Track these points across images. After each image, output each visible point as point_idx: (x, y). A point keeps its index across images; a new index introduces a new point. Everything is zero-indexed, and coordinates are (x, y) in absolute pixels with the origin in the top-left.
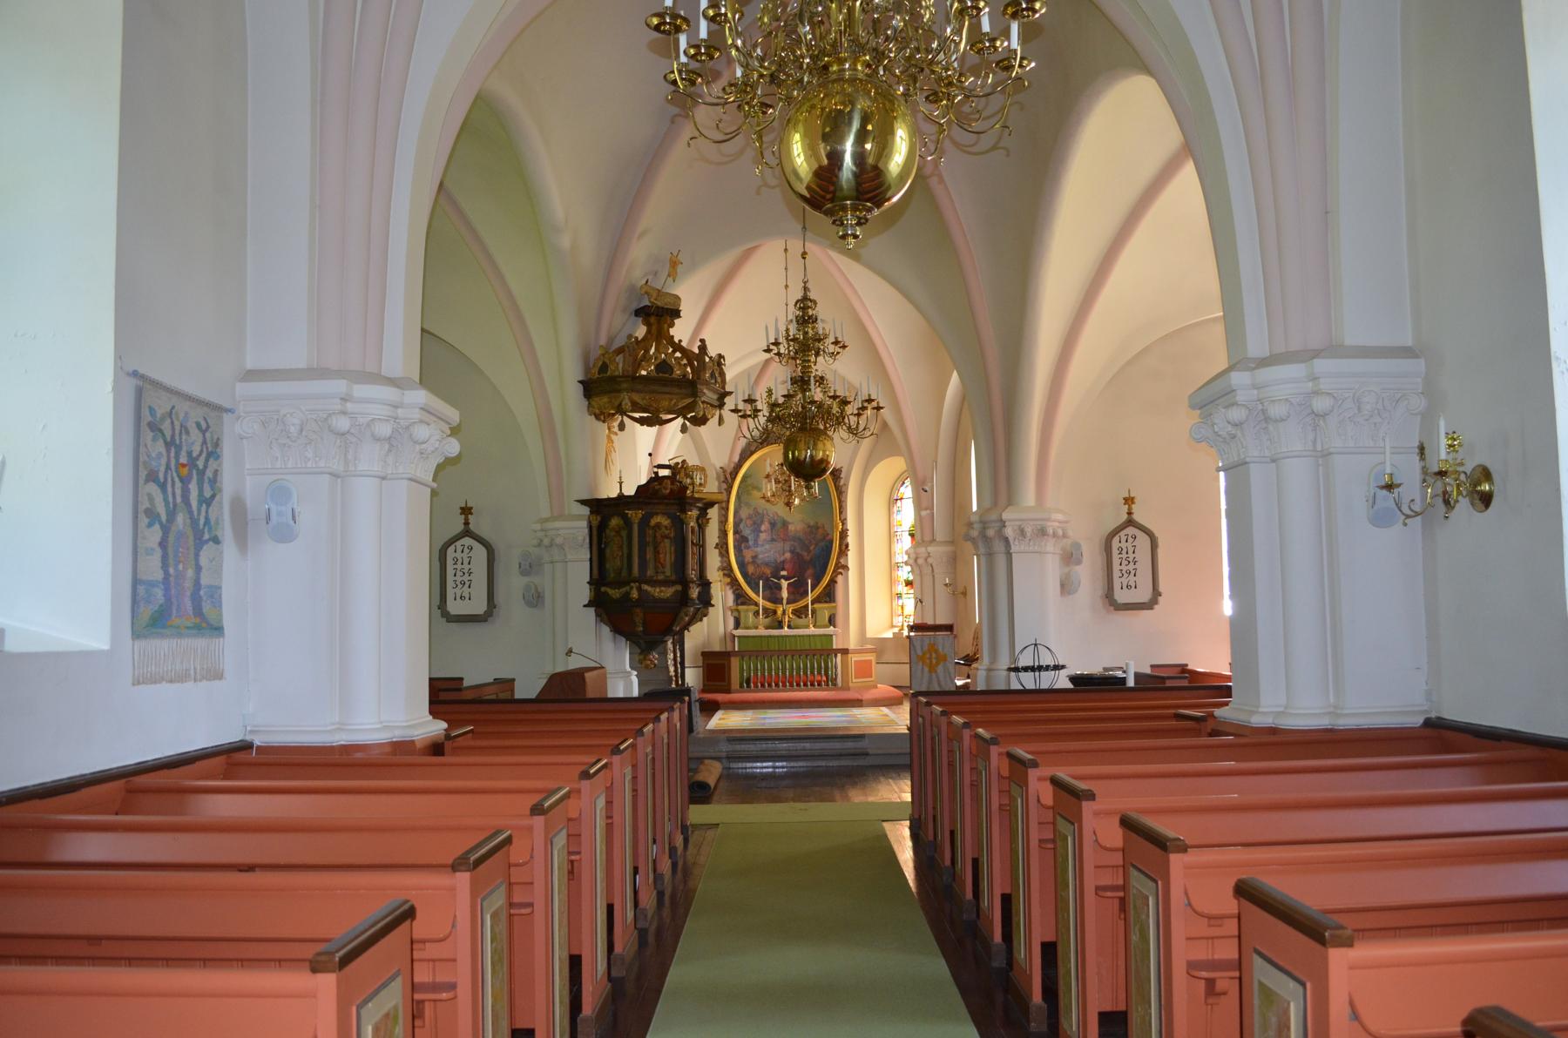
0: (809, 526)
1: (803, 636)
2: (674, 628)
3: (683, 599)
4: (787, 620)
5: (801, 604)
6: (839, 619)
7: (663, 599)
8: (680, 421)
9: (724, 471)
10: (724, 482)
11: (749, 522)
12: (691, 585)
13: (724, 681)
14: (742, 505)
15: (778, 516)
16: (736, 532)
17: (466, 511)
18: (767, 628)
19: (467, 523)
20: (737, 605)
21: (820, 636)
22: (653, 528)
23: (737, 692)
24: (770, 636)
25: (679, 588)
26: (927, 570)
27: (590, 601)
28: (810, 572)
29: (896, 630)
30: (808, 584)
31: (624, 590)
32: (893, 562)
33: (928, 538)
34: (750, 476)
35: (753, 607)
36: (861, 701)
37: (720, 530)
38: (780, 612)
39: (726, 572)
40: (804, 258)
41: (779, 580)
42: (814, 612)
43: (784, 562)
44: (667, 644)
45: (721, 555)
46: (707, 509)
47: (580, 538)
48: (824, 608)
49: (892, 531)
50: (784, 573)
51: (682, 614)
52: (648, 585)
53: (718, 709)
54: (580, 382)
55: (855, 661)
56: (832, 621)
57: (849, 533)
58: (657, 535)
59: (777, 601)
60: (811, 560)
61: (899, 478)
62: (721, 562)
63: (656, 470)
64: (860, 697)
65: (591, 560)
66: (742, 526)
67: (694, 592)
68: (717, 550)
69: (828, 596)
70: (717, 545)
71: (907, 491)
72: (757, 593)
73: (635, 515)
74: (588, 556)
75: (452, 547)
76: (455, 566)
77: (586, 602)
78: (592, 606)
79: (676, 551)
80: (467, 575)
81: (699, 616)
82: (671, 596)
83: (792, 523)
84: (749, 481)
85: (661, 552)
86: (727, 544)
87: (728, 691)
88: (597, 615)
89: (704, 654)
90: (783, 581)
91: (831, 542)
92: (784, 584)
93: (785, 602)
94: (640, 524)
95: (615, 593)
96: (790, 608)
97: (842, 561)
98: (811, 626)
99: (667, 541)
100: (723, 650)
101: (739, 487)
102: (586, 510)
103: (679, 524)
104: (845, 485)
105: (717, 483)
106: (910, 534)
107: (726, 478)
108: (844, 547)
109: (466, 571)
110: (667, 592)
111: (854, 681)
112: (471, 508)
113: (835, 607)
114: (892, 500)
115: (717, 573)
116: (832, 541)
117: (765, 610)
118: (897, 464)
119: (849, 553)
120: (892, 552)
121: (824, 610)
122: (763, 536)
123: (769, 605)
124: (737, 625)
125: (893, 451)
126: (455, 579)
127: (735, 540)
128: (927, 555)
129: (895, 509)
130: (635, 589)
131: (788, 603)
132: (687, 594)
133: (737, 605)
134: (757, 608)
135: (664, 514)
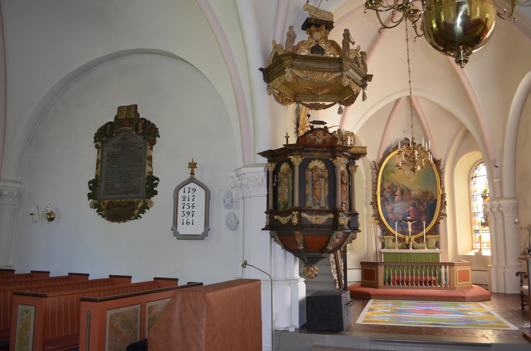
0: (423, 192)
1: (421, 253)
2: (328, 248)
3: (335, 225)
4: (411, 244)
5: (420, 235)
6: (442, 244)
7: (318, 225)
8: (337, 106)
9: (375, 163)
10: (374, 169)
11: (389, 190)
12: (341, 214)
13: (374, 280)
14: (385, 181)
15: (405, 187)
16: (381, 196)
17: (193, 165)
18: (400, 248)
19: (192, 173)
20: (383, 235)
21: (431, 253)
22: (312, 170)
23: (382, 288)
24: (402, 253)
25: (331, 216)
26: (499, 215)
27: (266, 226)
28: (424, 217)
29: (477, 251)
30: (423, 224)
31: (289, 217)
32: (472, 212)
33: (498, 195)
34: (389, 165)
35: (392, 237)
36: (465, 297)
37: (373, 194)
38: (407, 239)
39: (377, 217)
40: (410, 83)
41: (407, 222)
42: (426, 240)
43: (409, 212)
44: (329, 259)
45: (374, 208)
46: (354, 159)
47: (260, 180)
48: (433, 238)
49: (471, 195)
50: (409, 218)
51: (334, 237)
52: (307, 213)
53: (371, 298)
54: (261, 69)
55: (458, 271)
56: (437, 245)
57: (446, 196)
58: (314, 175)
59: (405, 233)
60: (425, 210)
61: (474, 164)
62: (374, 212)
63: (311, 124)
64: (463, 295)
65: (268, 195)
66: (385, 193)
67: (343, 220)
68: (371, 206)
69: (435, 231)
70: (371, 202)
71: (482, 170)
72: (394, 229)
73: (296, 160)
74: (266, 193)
75: (182, 189)
76: (184, 202)
77: (264, 227)
78: (267, 230)
79: (329, 187)
80: (191, 207)
81: (349, 238)
82: (325, 222)
83: (413, 191)
84: (389, 168)
85: (317, 188)
86: (377, 202)
87: (377, 287)
88: (272, 237)
89: (363, 264)
90: (409, 222)
91: (436, 201)
92: (410, 224)
93: (410, 234)
94: (300, 166)
95: (284, 220)
96: (413, 238)
97: (443, 211)
98: (426, 248)
99: (322, 180)
100: (376, 261)
101: (383, 172)
102: (265, 160)
103: (331, 168)
104: (443, 169)
105: (371, 170)
106: (482, 197)
107: (376, 167)
108: (443, 203)
109: (191, 205)
110: (322, 219)
111: (458, 284)
112: (196, 164)
113: (439, 237)
114: (470, 178)
115: (372, 218)
116: (437, 200)
117: (399, 238)
118: (476, 155)
119: (447, 207)
120: (471, 207)
121: (433, 239)
122: (397, 198)
123: (401, 236)
124: (383, 246)
125: (473, 147)
126: (183, 210)
127: (381, 200)
128: (498, 205)
129: (472, 183)
130: (295, 216)
131: (412, 235)
132: (338, 221)
133: (383, 235)
134: (394, 237)
135: (319, 160)
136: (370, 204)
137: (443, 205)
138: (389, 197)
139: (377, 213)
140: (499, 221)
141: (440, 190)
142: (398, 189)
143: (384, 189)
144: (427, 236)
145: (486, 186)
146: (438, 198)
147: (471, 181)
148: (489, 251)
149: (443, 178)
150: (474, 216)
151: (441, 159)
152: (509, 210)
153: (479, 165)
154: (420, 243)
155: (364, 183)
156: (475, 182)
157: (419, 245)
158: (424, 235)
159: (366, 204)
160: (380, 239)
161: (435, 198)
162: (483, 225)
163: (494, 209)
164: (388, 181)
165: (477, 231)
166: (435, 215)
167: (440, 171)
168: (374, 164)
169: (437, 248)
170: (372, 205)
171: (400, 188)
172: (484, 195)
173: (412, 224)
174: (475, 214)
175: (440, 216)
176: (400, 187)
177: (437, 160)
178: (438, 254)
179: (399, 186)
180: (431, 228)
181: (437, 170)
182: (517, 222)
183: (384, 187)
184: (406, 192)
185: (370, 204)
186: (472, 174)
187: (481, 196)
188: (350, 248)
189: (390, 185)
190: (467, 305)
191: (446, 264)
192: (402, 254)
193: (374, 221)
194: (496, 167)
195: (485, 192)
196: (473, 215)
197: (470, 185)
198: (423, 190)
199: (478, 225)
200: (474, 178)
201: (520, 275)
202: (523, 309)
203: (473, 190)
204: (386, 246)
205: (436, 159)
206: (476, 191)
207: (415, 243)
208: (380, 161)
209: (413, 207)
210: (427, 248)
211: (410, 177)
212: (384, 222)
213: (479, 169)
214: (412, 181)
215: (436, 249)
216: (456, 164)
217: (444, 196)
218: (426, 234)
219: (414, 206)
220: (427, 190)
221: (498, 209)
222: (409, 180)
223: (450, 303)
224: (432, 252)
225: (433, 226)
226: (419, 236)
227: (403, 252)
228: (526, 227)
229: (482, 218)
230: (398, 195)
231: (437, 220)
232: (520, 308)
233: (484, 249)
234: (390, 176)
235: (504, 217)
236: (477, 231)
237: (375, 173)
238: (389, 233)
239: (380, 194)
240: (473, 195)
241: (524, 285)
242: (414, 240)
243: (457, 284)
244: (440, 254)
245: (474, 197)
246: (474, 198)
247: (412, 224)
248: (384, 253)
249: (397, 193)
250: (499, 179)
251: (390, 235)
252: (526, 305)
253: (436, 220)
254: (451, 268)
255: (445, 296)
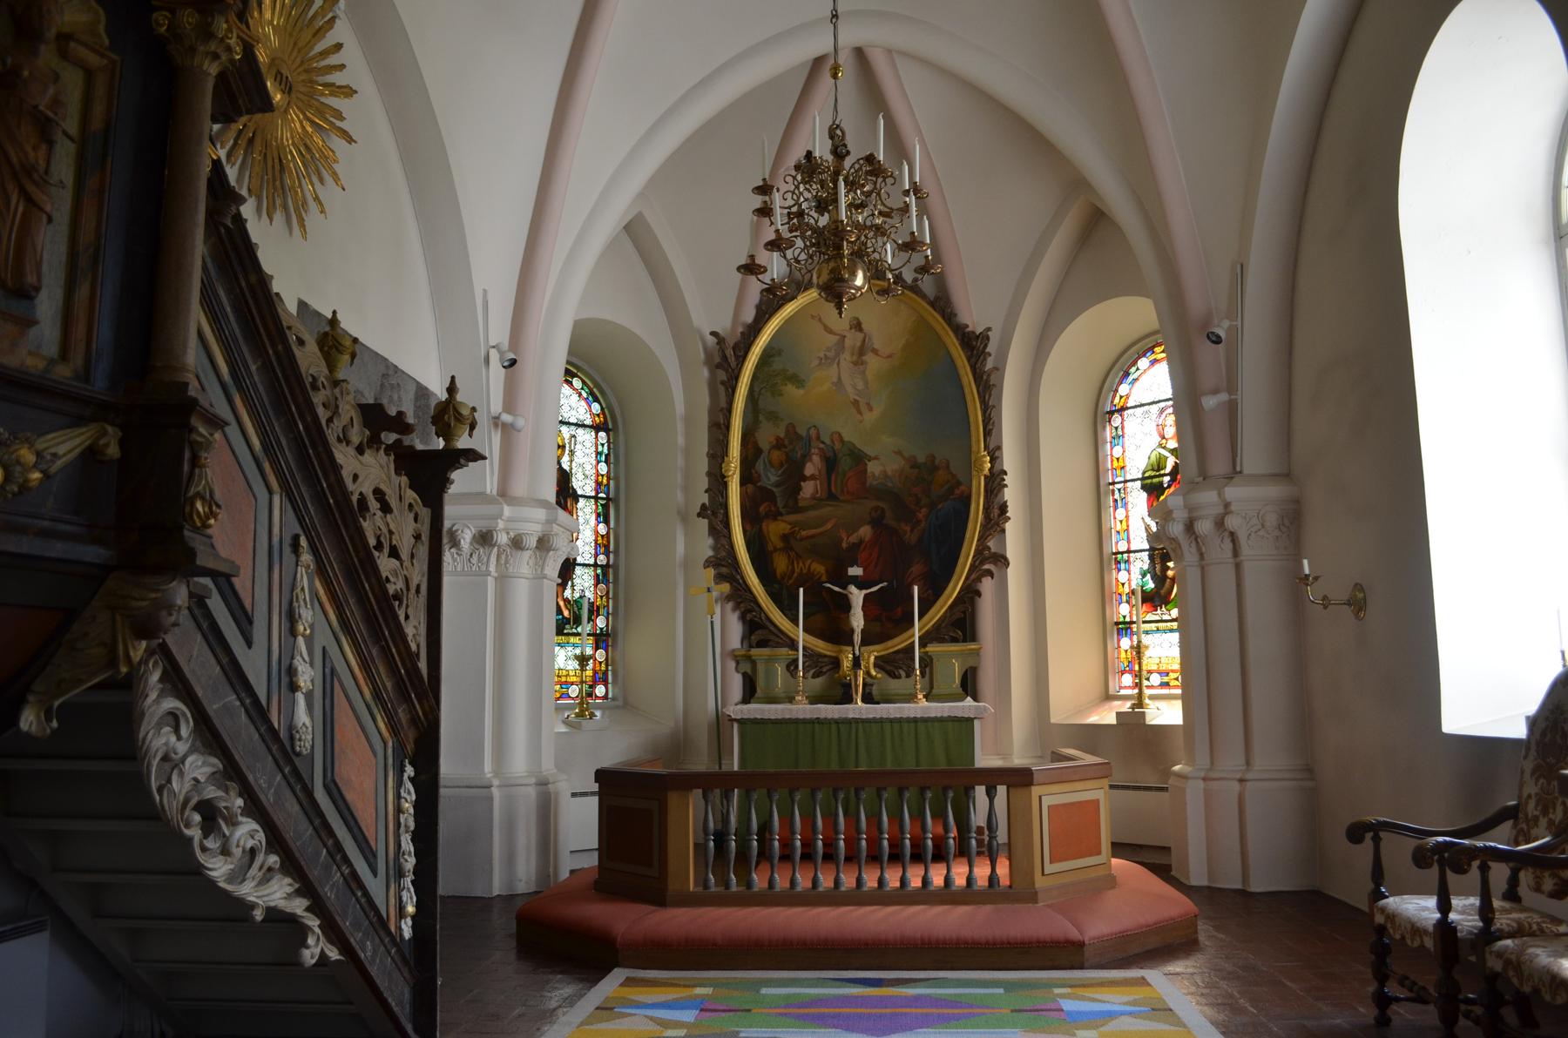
1: (900, 721)
5: (897, 644)
6: (987, 681)
10: (718, 366)
11: (777, 456)
14: (761, 418)
18: (814, 700)
21: (941, 720)
24: (818, 721)
26: (1220, 551)
29: (1126, 707)
33: (1219, 465)
34: (779, 353)
35: (784, 651)
38: (847, 663)
39: (724, 570)
45: (713, 531)
49: (1102, 483)
56: (969, 685)
57: (1008, 480)
62: (715, 548)
64: (1074, 934)
66: (760, 466)
69: (962, 625)
83: (876, 458)
84: (778, 364)
86: (725, 506)
87: (659, 898)
90: (853, 588)
91: (966, 500)
92: (857, 596)
93: (857, 638)
96: (871, 655)
98: (920, 696)
101: (755, 378)
104: (996, 369)
105: (705, 373)
106: (1144, 487)
107: (725, 357)
108: (996, 512)
111: (1051, 872)
113: (977, 653)
116: (969, 497)
119: (1008, 526)
123: (821, 646)
124: (749, 694)
128: (1221, 510)
131: (864, 643)
136: (699, 515)
137: (996, 516)
138: (778, 485)
139: (724, 554)
140: (1222, 577)
141: (984, 456)
142: (813, 450)
143: (759, 452)
144: (927, 649)
145: (1160, 445)
146: (974, 490)
147: (1104, 428)
148: (1178, 705)
149: (994, 407)
150: (1114, 567)
151: (989, 329)
152: (1263, 526)
153: (1135, 363)
154: (899, 677)
155: (680, 427)
156: (1120, 430)
157: (895, 685)
158: (914, 642)
159: (684, 517)
160: (738, 663)
161: (962, 488)
162: (1153, 599)
163: (1204, 527)
164: (774, 417)
165: (1125, 628)
166: (961, 560)
167: (985, 377)
168: (718, 343)
169: (969, 698)
170: (706, 521)
171: (822, 446)
172: (1156, 480)
173: (866, 596)
174: (1119, 556)
175: (982, 563)
176: (823, 443)
177: (973, 332)
178: (965, 724)
179: (818, 438)
180: (946, 611)
181: (974, 374)
182: (1307, 576)
183: (756, 443)
184: (845, 463)
185: (699, 515)
186: (1106, 398)
187: (1139, 483)
188: (620, 703)
189: (782, 435)
190: (1088, 993)
191: (991, 778)
192: (817, 725)
193: (712, 584)
194: (1214, 342)
195: (1158, 470)
196: (1110, 560)
197: (1100, 442)
198: (914, 457)
199: (1128, 602)
200: (1116, 415)
201: (1369, 835)
202: (1383, 1021)
203: (1112, 461)
204: (759, 690)
205: (969, 329)
206: (1123, 468)
207: (879, 676)
208: (742, 333)
209: (873, 527)
210: (925, 696)
211: (862, 401)
212: (754, 589)
213: (1135, 376)
214: (870, 417)
215: (962, 700)
216: (1052, 347)
217: (998, 480)
218: (924, 642)
219: (877, 522)
220: (932, 458)
221: (1220, 524)
222: (861, 413)
223: (1009, 986)
224: (946, 715)
225: (951, 607)
226: (896, 648)
227: (822, 716)
228: (1346, 597)
229: (1144, 576)
230: (813, 477)
231: (969, 582)
232: (1367, 1013)
233: (1152, 697)
234: (781, 395)
235: (1242, 558)
236: (1125, 628)
237: (723, 383)
238: (772, 637)
239: (738, 471)
240: (1111, 481)
241: (1392, 895)
242: (875, 665)
243: (1043, 874)
244: (976, 723)
245: (1113, 491)
246: (1113, 495)
247: (866, 595)
248: (741, 722)
249: (809, 470)
250: (1224, 397)
251: (778, 645)
252: (1398, 1000)
253: (967, 578)
254: (1018, 793)
255: (987, 943)
